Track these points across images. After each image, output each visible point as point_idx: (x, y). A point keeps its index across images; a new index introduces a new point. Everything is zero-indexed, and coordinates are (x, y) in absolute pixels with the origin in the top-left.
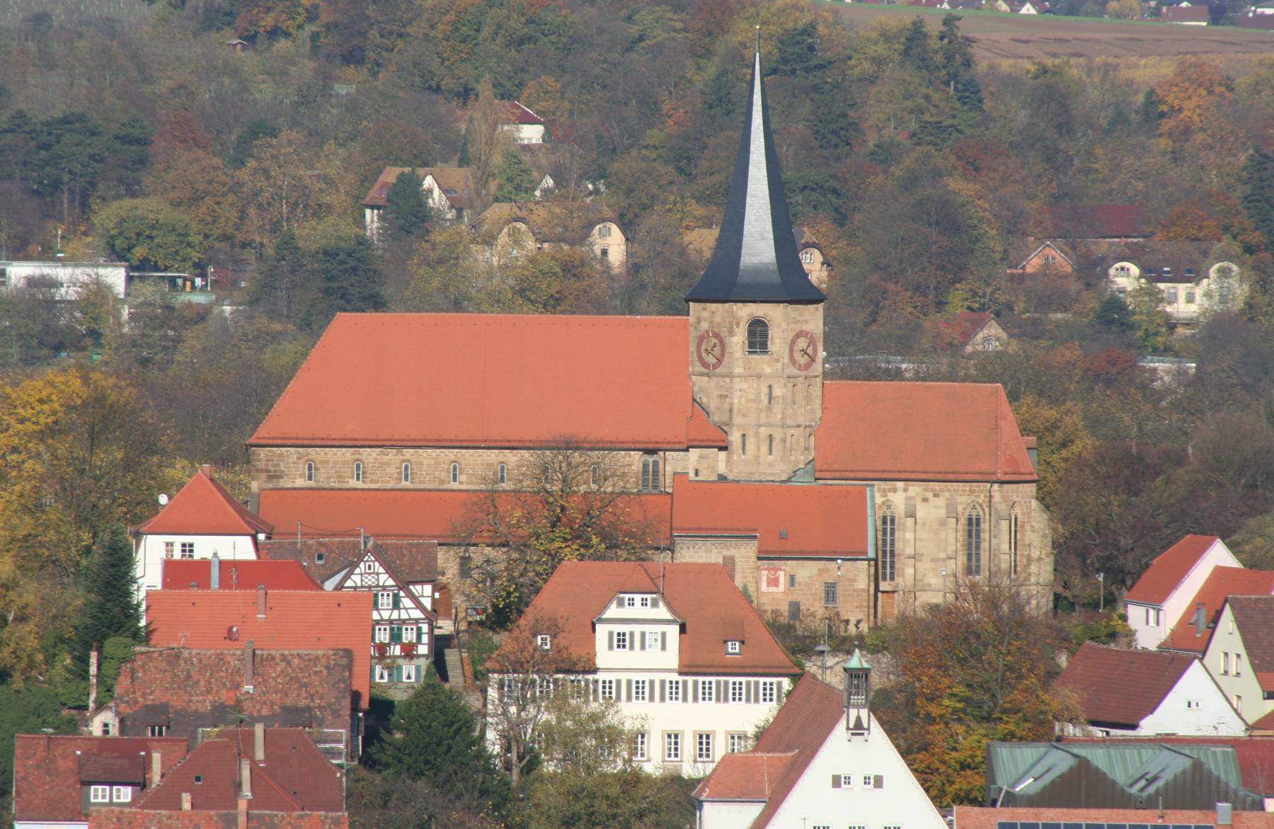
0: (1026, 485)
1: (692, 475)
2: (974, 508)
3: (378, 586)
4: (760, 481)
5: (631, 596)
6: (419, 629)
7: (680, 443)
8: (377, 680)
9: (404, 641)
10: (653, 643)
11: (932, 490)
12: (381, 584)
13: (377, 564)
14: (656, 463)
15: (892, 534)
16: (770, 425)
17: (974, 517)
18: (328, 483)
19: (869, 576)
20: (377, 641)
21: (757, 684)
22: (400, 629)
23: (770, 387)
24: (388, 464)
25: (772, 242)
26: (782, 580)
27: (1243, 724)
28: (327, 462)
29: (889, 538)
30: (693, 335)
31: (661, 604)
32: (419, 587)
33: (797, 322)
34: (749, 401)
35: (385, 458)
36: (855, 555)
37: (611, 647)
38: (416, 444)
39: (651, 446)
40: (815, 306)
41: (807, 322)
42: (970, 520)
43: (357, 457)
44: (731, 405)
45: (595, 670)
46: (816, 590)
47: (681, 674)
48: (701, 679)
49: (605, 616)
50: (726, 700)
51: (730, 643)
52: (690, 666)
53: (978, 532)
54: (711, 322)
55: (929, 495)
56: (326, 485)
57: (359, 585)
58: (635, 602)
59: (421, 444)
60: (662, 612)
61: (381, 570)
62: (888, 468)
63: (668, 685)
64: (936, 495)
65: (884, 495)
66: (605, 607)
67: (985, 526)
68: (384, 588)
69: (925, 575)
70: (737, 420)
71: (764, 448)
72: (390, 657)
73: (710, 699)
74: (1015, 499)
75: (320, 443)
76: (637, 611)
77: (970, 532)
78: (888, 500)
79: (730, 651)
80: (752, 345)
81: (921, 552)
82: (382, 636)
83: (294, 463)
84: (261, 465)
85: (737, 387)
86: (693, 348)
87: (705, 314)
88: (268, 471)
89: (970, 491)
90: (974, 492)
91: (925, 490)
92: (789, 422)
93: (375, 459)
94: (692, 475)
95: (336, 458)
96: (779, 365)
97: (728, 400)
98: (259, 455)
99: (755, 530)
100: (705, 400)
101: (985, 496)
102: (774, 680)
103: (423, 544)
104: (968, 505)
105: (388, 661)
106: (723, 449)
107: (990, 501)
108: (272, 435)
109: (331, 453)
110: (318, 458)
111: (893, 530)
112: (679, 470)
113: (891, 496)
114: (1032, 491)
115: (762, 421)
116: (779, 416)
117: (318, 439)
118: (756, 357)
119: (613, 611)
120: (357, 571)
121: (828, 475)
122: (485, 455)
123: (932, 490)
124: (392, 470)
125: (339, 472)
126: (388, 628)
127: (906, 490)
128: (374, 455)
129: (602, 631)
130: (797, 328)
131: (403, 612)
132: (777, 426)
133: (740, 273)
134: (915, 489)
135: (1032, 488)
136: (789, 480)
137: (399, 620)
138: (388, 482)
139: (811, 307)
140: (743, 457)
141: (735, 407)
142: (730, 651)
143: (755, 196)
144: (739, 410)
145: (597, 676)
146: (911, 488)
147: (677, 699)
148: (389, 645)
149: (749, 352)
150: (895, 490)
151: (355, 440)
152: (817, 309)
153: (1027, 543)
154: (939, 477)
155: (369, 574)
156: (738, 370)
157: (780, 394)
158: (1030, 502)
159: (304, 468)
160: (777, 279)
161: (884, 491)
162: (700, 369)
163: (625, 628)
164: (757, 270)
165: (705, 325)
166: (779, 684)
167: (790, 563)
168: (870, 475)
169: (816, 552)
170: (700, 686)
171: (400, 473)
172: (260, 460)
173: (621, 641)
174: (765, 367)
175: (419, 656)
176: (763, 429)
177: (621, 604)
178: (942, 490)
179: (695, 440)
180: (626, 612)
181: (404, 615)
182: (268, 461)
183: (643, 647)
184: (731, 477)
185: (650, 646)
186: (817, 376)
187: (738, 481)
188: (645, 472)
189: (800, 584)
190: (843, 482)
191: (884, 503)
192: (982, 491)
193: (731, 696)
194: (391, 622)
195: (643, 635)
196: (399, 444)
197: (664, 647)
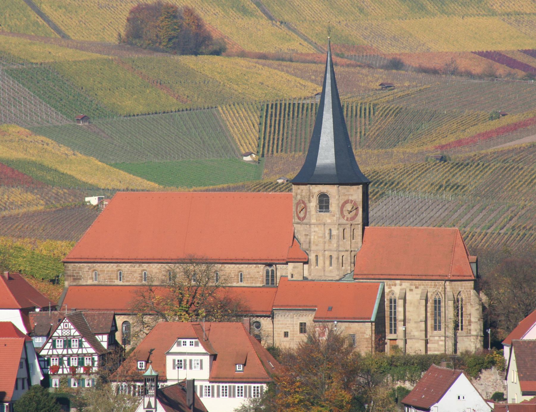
1: (289, 277)
2: (437, 294)
3: (70, 336)
4: (325, 280)
5: (184, 340)
6: (93, 359)
7: (284, 260)
8: (72, 386)
9: (85, 365)
10: (196, 365)
11: (415, 285)
12: (72, 335)
13: (70, 324)
14: (272, 271)
15: (395, 308)
16: (330, 250)
17: (437, 299)
18: (104, 282)
19: (372, 330)
20: (85, 365)
21: (250, 387)
22: (83, 359)
23: (330, 230)
24: (135, 272)
27: (490, 408)
28: (104, 271)
29: (393, 311)
30: (295, 202)
31: (200, 344)
32: (100, 337)
33: (345, 195)
34: (319, 237)
35: (133, 269)
36: (364, 320)
38: (148, 261)
39: (268, 262)
40: (358, 186)
41: (352, 195)
42: (435, 301)
43: (119, 268)
44: (310, 239)
45: (166, 381)
47: (211, 382)
48: (221, 385)
50: (234, 396)
51: (237, 366)
52: (215, 378)
53: (440, 307)
54: (301, 195)
55: (413, 287)
56: (103, 284)
57: (61, 335)
59: (151, 261)
60: (201, 349)
61: (72, 327)
62: (392, 273)
63: (204, 388)
64: (417, 288)
65: (390, 288)
66: (171, 347)
67: (443, 304)
68: (74, 337)
69: (412, 331)
70: (313, 247)
71: (327, 263)
72: (78, 374)
73: (242, 396)
74: (460, 290)
75: (99, 261)
76: (188, 348)
77: (435, 307)
78: (392, 291)
79: (238, 369)
80: (321, 207)
81: (410, 318)
82: (74, 362)
83: (87, 272)
84: (69, 273)
85: (312, 230)
86: (294, 209)
87: (299, 191)
88: (74, 276)
89: (434, 285)
90: (437, 285)
91: (411, 285)
92: (341, 249)
93: (128, 269)
94: (289, 277)
95: (108, 269)
96: (335, 218)
97: (308, 237)
98: (68, 267)
99: (316, 306)
100: (299, 237)
101: (442, 288)
102: (259, 385)
103: (106, 314)
104: (434, 293)
105: (77, 376)
106: (306, 263)
107: (445, 291)
108: (75, 257)
109: (106, 266)
110: (99, 269)
111: (395, 306)
112: (284, 275)
113: (393, 288)
114: (471, 286)
115: (327, 247)
116: (335, 245)
117: (99, 259)
118: (322, 213)
119: (175, 349)
120: (60, 328)
121: (360, 277)
122: (106, 266)
123: (415, 285)
124: (137, 275)
125: (110, 276)
126: (77, 358)
127: (401, 285)
128: (128, 267)
129: (169, 359)
130: (346, 198)
131: (84, 350)
132: (334, 251)
133: (316, 169)
134: (406, 284)
135: (472, 284)
136: (340, 280)
137: (82, 354)
138: (135, 281)
139: (355, 187)
140: (316, 267)
141: (312, 240)
142: (238, 369)
144: (314, 242)
146: (403, 284)
147: (226, 396)
148: (77, 367)
149: (320, 211)
150: (395, 285)
151: (117, 259)
152: (358, 188)
153: (468, 313)
154: (418, 278)
155: (66, 329)
156: (313, 221)
157: (335, 234)
158: (470, 291)
159: (92, 275)
160: (334, 172)
161: (390, 285)
162: (297, 220)
165: (299, 197)
166: (262, 387)
168: (382, 277)
169: (345, 318)
170: (221, 388)
171: (141, 277)
172: (70, 270)
174: (327, 219)
175: (93, 373)
176: (326, 252)
177: (179, 344)
178: (420, 285)
179: (291, 258)
180: (182, 349)
181: (85, 351)
182: (73, 270)
183: (191, 368)
184: (310, 278)
185: (195, 367)
186: (358, 224)
187: (314, 280)
188: (267, 276)
190: (368, 281)
191: (390, 292)
192: (440, 285)
193: (237, 394)
194: (78, 355)
195: (191, 361)
196: (140, 261)
197: (201, 368)
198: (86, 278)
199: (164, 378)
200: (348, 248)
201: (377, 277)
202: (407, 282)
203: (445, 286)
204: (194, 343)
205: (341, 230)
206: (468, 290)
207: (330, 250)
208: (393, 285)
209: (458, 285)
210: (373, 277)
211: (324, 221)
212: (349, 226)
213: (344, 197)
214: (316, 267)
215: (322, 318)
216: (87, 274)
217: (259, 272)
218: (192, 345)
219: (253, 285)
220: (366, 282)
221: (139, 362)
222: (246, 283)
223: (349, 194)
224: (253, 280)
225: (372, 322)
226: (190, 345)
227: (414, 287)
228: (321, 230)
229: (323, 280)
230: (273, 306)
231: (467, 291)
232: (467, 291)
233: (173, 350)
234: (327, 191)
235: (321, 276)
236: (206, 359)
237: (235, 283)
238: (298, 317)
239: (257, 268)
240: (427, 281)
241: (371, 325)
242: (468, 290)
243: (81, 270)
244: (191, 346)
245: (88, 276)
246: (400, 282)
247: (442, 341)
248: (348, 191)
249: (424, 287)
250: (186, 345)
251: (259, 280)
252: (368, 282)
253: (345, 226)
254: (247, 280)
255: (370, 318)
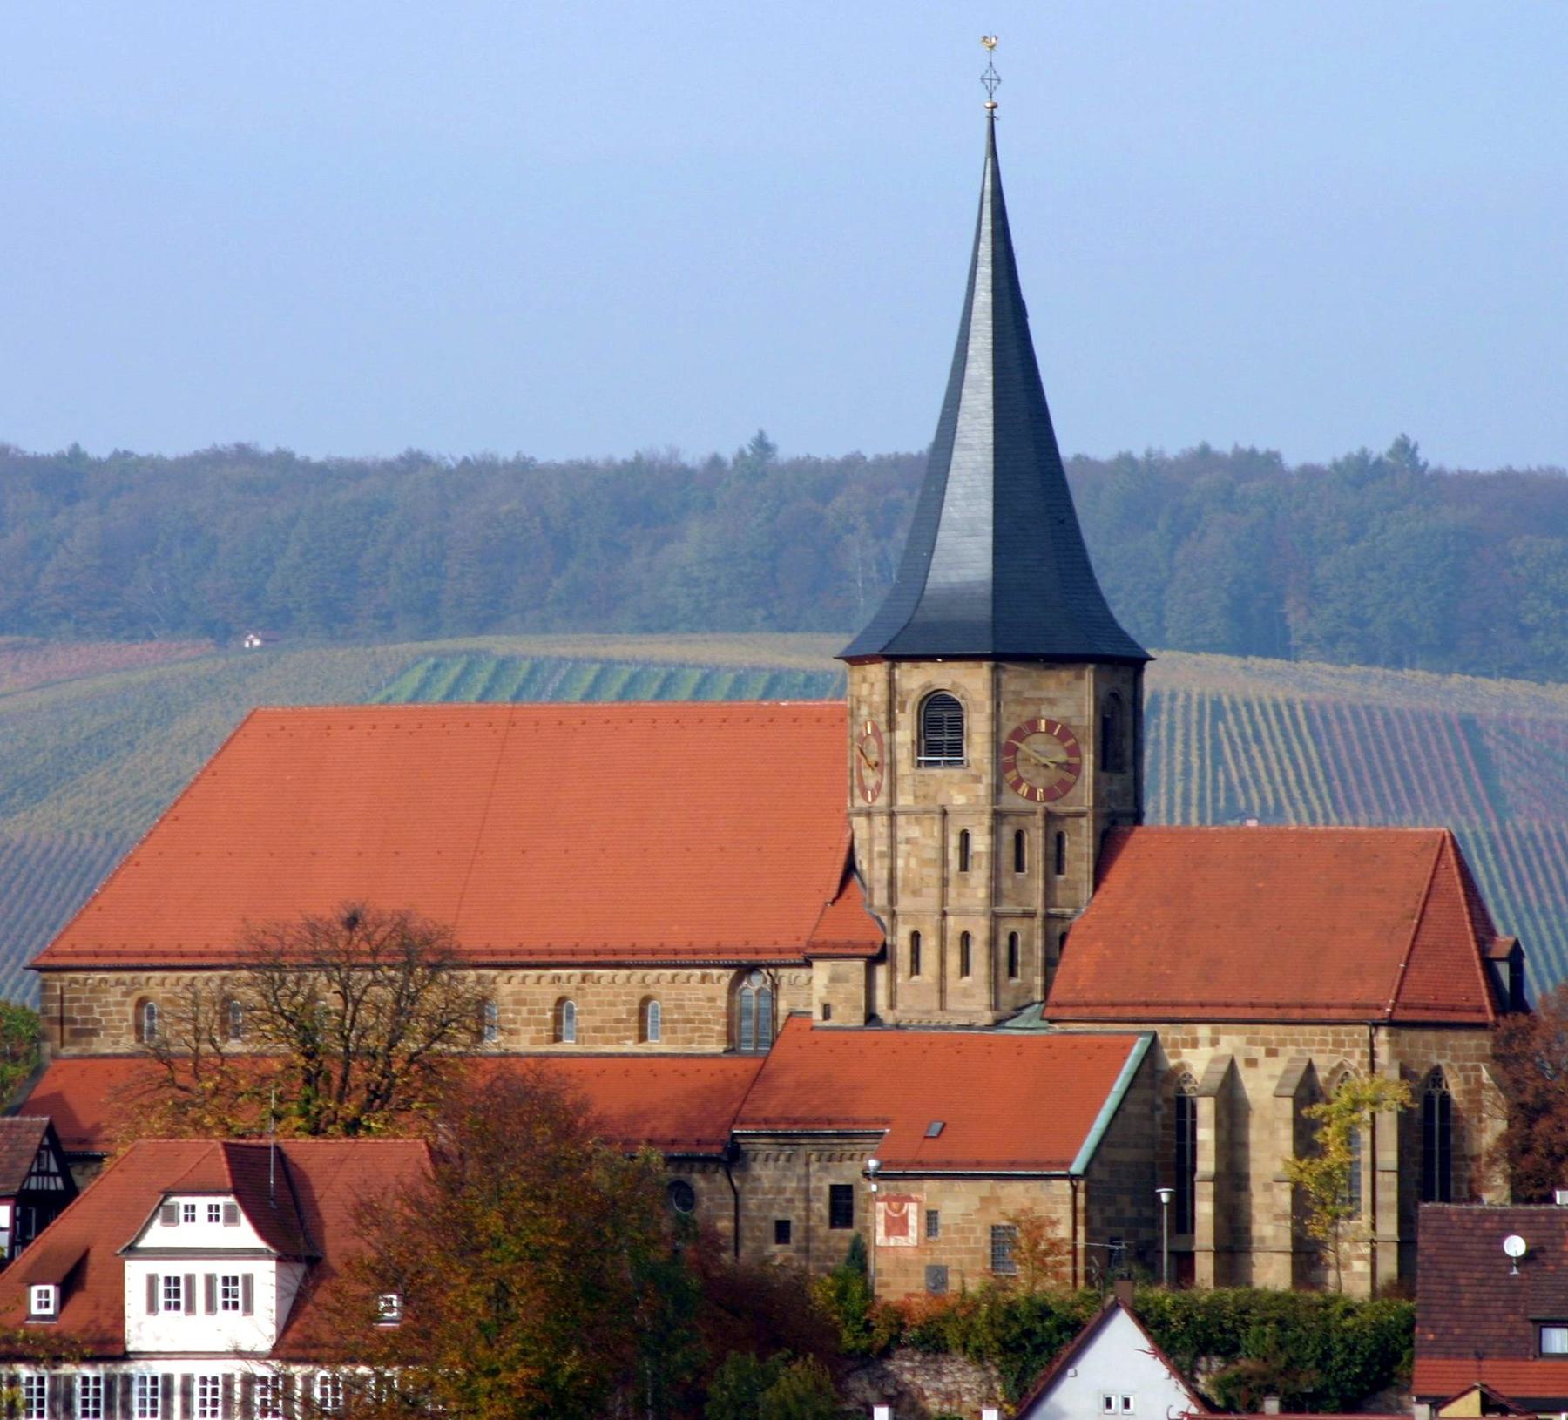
0: (1463, 1035)
1: (817, 1015)
11: (1265, 1042)
25: (988, 540)
26: (913, 1220)
31: (243, 1218)
33: (1024, 702)
37: (152, 1308)
39: (745, 958)
45: (126, 1357)
46: (977, 1241)
49: (143, 1244)
55: (1259, 1052)
58: (197, 1213)
60: (244, 1234)
64: (1271, 1053)
70: (904, 903)
71: (954, 960)
91: (1251, 1042)
92: (1005, 908)
99: (886, 1122)
101: (1363, 1053)
103: (18, 1126)
112: (801, 1008)
116: (982, 893)
118: (937, 772)
119: (158, 1235)
123: (1265, 1042)
127: (1214, 1042)
129: (136, 1273)
134: (1232, 1041)
139: (1066, 675)
143: (969, 447)
144: (905, 880)
145: (125, 1368)
150: (1194, 1043)
158: (1478, 1069)
160: (984, 612)
163: (178, 1268)
164: (955, 595)
167: (928, 1185)
168: (1144, 1013)
173: (176, 1295)
174: (953, 792)
177: (170, 1218)
178: (1282, 1043)
179: (824, 944)
186: (1081, 815)
189: (947, 1227)
190: (1097, 1027)
192: (1356, 1044)
198: (116, 1028)
199: (119, 1352)
200: (1037, 904)
201: (1129, 1012)
202: (1238, 1033)
203: (1372, 1045)
204: (221, 1213)
205: (1008, 833)
206: (1469, 1064)
207: (964, 913)
208: (1185, 1046)
209: (1427, 1045)
210: (1112, 1013)
211: (941, 800)
212: (1039, 820)
213: (1018, 709)
214: (915, 978)
215: (898, 1165)
216: (118, 1012)
217: (711, 1000)
218: (217, 1218)
219: (695, 1048)
220: (1088, 1033)
221: (35, 1290)
222: (669, 1042)
223: (1040, 699)
224: (693, 1030)
225: (1072, 1177)
226: (210, 1218)
227: (1263, 1049)
228: (932, 836)
229: (935, 1028)
230: (734, 1122)
231: (1462, 1069)
232: (1462, 1069)
233: (145, 1243)
234: (954, 684)
235: (929, 1012)
236: (265, 1274)
237: (630, 1042)
238: (825, 1163)
239: (708, 985)
240: (1307, 1029)
241: (1070, 1192)
242: (1469, 1064)
243: (98, 1000)
244: (214, 1224)
245: (121, 1021)
246: (1214, 1032)
247: (1361, 1257)
248: (1035, 687)
249: (1299, 1052)
250: (193, 1219)
251: (712, 1030)
252: (1095, 1033)
253: (1023, 819)
254: (674, 1031)
255: (1068, 1164)
